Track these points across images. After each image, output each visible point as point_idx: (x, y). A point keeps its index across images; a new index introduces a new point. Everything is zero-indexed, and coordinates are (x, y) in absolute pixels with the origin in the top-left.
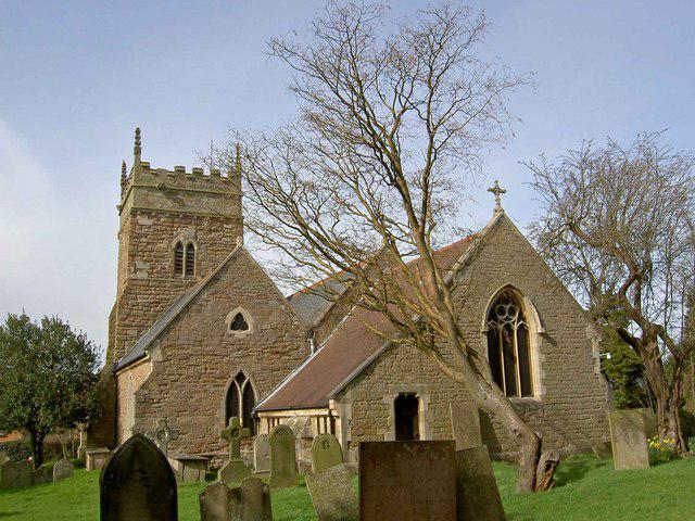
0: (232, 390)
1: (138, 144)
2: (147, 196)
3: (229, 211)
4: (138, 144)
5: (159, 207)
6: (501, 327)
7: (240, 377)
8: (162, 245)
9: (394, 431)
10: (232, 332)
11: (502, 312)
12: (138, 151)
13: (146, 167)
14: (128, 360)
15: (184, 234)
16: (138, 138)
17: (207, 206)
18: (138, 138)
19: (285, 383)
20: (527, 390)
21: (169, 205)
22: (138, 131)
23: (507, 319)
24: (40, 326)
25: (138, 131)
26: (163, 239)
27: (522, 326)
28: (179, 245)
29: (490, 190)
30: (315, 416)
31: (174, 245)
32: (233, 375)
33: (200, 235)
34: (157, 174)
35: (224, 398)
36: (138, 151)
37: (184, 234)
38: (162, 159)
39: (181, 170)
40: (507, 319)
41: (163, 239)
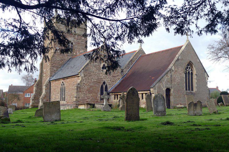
6: (187, 72)
7: (104, 83)
11: (188, 68)
20: (192, 90)
23: (189, 70)
27: (192, 72)
30: (141, 93)
32: (102, 82)
33: (75, 40)
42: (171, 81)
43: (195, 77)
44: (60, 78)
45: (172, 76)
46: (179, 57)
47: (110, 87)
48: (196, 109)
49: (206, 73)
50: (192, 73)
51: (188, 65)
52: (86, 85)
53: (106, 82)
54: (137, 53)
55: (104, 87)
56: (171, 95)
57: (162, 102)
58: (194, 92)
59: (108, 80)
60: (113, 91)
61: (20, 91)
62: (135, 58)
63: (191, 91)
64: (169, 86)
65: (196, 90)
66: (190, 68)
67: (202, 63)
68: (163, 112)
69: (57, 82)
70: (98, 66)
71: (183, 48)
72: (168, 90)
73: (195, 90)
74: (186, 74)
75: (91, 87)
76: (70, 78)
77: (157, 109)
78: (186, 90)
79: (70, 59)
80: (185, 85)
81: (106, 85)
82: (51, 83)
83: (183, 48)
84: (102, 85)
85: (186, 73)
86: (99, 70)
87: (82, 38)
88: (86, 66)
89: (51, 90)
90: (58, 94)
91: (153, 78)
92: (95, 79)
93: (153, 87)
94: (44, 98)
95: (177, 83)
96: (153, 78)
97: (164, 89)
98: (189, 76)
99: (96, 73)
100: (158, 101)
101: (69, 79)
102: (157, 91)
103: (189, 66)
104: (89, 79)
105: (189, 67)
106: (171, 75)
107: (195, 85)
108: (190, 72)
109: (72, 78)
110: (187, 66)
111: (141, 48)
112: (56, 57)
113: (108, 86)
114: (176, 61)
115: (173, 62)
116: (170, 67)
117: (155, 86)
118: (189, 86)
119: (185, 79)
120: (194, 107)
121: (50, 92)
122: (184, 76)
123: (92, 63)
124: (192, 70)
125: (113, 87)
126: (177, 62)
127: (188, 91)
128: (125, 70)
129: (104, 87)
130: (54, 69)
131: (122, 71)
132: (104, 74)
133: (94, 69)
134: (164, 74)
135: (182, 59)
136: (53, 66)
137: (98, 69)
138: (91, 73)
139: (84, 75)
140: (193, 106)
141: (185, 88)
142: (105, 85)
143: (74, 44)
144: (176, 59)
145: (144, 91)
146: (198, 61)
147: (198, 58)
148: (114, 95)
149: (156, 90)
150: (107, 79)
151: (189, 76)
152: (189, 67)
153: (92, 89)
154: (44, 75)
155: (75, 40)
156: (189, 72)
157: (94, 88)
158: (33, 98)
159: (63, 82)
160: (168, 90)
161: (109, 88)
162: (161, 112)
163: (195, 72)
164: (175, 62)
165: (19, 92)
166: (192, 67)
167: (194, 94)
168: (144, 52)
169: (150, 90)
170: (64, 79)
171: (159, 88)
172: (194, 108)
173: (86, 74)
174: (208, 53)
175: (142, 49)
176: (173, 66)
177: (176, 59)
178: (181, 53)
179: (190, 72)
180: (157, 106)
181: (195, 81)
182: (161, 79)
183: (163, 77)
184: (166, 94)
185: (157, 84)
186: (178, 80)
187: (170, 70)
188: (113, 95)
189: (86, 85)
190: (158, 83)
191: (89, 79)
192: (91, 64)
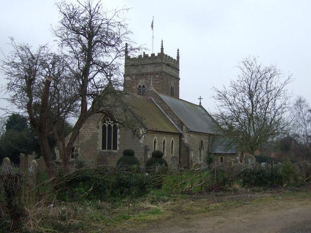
5: (132, 72)
12: (162, 49)
15: (141, 82)
20: (115, 148)
21: (135, 71)
28: (140, 86)
39: (146, 56)
78: (104, 148)
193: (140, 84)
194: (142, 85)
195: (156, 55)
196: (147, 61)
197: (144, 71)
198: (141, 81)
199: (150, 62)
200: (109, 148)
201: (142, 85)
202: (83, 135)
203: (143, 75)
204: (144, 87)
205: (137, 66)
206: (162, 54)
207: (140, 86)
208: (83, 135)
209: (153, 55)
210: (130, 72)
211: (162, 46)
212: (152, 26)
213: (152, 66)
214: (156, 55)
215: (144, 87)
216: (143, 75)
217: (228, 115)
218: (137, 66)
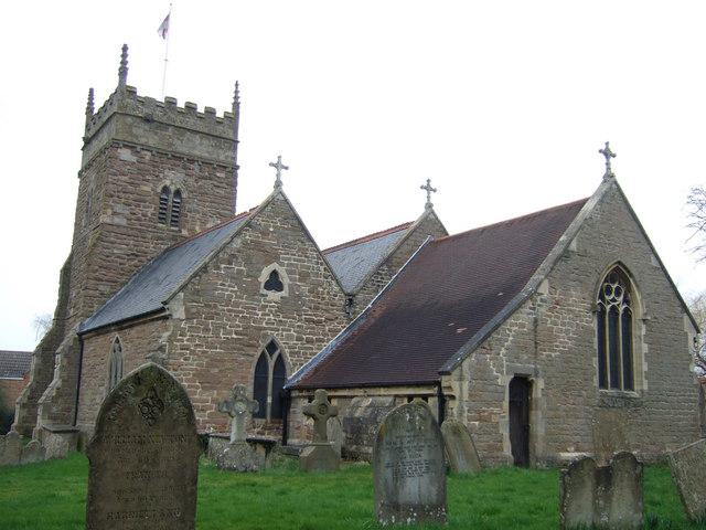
0: (262, 361)
1: (124, 63)
2: (131, 126)
3: (222, 156)
4: (124, 63)
5: (143, 140)
6: (608, 308)
7: (272, 347)
8: (145, 188)
9: (507, 419)
10: (265, 292)
11: (609, 293)
12: (123, 72)
13: (132, 92)
14: (96, 324)
15: (173, 178)
16: (124, 56)
17: (201, 148)
18: (124, 56)
19: (607, 318)
20: (629, 386)
21: (153, 141)
22: (125, 48)
23: (613, 300)
24: (250, 194)
25: (125, 48)
26: (148, 181)
27: (626, 310)
28: (166, 190)
29: (600, 151)
30: (405, 396)
31: (159, 190)
32: (263, 345)
33: (191, 181)
34: (147, 101)
35: (253, 370)
36: (123, 72)
37: (173, 178)
38: (150, 85)
39: (171, 102)
40: (613, 300)
41: (148, 181)
42: (537, 338)
43: (639, 330)
44: (109, 325)
45: (540, 322)
46: (570, 243)
47: (295, 365)
48: (608, 499)
49: (686, 317)
50: (627, 315)
51: (611, 278)
52: (193, 352)
53: (281, 343)
54: (415, 230)
55: (271, 363)
56: (534, 406)
57: (424, 455)
58: (635, 394)
59: (290, 337)
60: (304, 379)
61: (13, 372)
62: (405, 248)
63: (626, 388)
64: (525, 367)
65: (645, 387)
66: (618, 293)
67: (675, 282)
68: (434, 507)
69: (101, 339)
70: (248, 276)
71: (588, 207)
72: (521, 385)
73: (642, 384)
74: (601, 315)
75: (214, 361)
76: (140, 324)
77: (396, 492)
78: (603, 384)
79: (166, 251)
80: (596, 365)
81: (280, 356)
82: (85, 342)
83: (588, 207)
84: (263, 354)
85: (603, 312)
86: (253, 292)
87: (218, 175)
88: (195, 275)
89: (84, 371)
90: (101, 388)
91: (459, 331)
92: (231, 329)
93: (454, 368)
94: (54, 399)
95: (562, 352)
96: (459, 331)
97: (504, 380)
98: (614, 329)
99: (237, 305)
100: (400, 450)
101: (138, 328)
102: (471, 389)
103: (616, 285)
104: (208, 330)
105: (614, 286)
106: (536, 321)
107: (641, 365)
108: (621, 309)
109: (144, 323)
110: (606, 281)
111: (433, 212)
112: (112, 243)
113: (289, 360)
114: (559, 258)
115: (545, 265)
116: (529, 287)
117: (460, 365)
118: (615, 364)
119: (596, 340)
120: (595, 491)
121: (80, 378)
122: (595, 325)
123: (223, 266)
124: (626, 301)
125: (310, 364)
126: (561, 265)
127: (610, 391)
128: (360, 296)
129: (271, 363)
130: (101, 288)
131: (351, 300)
132: (271, 312)
133: (230, 290)
134: (504, 312)
135: (583, 254)
136: (96, 279)
137: (246, 291)
138: (215, 307)
139: (187, 310)
140: (589, 484)
141: (596, 380)
142: (277, 353)
143: (184, 196)
144: (557, 250)
145: (418, 385)
146: (654, 263)
147: (653, 249)
148: (305, 397)
149: (466, 385)
150: (283, 330)
151: (614, 329)
152: (614, 286)
153: (217, 370)
154: (71, 312)
155: (191, 181)
156: (614, 309)
157: (228, 365)
158: (25, 400)
159: (117, 341)
160: (521, 385)
161: (292, 371)
162: (420, 508)
163: (639, 311)
164: (555, 264)
165: (11, 374)
166: (629, 289)
167: (637, 405)
168: (442, 226)
169: (438, 384)
170: (121, 329)
171: (481, 374)
172: (596, 498)
173: (194, 310)
174: (690, 226)
175: (435, 215)
176: (546, 282)
177: (557, 250)
178: (581, 228)
179: (621, 309)
180: (398, 476)
181: (641, 348)
182: (489, 335)
183: (498, 326)
184: (510, 402)
185: (469, 354)
186: (564, 341)
187: (531, 297)
188: (301, 397)
189: (193, 352)
190: (474, 350)
191: (208, 330)
192: (218, 268)
193: (168, 183)
194: (173, 188)
195: (220, 114)
196: (191, 122)
197: (182, 147)
198: (171, 174)
199: (200, 126)
200: (615, 384)
201: (173, 188)
202: (551, 330)
203: (180, 159)
204: (178, 193)
205: (164, 126)
206: (125, 92)
207: (166, 190)
208: (551, 330)
209: (210, 112)
210: (137, 137)
211: (236, 98)
212: (164, 30)
213: (205, 142)
214: (220, 114)
215: (178, 193)
216: (180, 159)
217: (573, 507)
218: (164, 126)
